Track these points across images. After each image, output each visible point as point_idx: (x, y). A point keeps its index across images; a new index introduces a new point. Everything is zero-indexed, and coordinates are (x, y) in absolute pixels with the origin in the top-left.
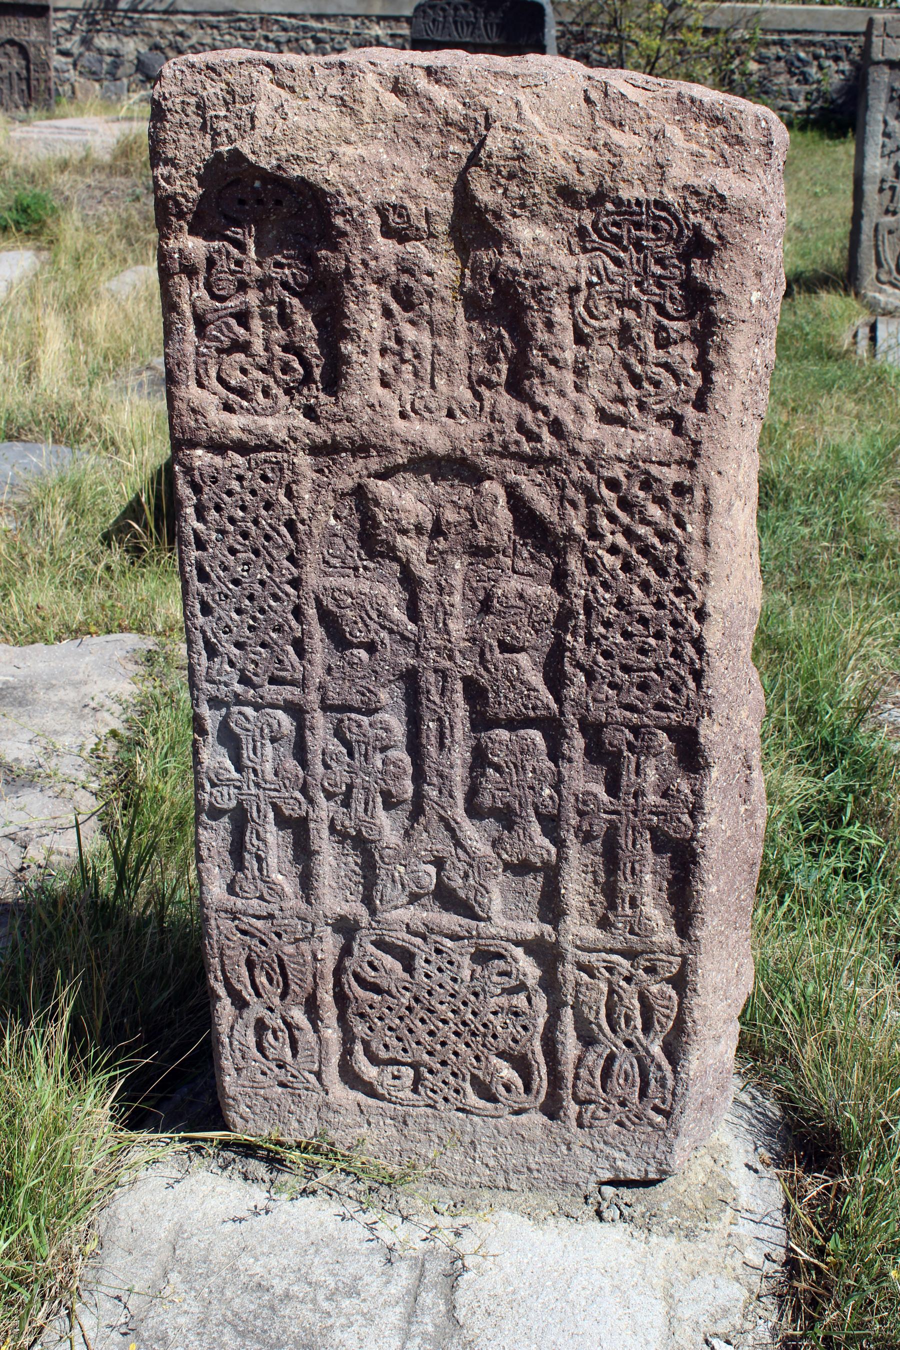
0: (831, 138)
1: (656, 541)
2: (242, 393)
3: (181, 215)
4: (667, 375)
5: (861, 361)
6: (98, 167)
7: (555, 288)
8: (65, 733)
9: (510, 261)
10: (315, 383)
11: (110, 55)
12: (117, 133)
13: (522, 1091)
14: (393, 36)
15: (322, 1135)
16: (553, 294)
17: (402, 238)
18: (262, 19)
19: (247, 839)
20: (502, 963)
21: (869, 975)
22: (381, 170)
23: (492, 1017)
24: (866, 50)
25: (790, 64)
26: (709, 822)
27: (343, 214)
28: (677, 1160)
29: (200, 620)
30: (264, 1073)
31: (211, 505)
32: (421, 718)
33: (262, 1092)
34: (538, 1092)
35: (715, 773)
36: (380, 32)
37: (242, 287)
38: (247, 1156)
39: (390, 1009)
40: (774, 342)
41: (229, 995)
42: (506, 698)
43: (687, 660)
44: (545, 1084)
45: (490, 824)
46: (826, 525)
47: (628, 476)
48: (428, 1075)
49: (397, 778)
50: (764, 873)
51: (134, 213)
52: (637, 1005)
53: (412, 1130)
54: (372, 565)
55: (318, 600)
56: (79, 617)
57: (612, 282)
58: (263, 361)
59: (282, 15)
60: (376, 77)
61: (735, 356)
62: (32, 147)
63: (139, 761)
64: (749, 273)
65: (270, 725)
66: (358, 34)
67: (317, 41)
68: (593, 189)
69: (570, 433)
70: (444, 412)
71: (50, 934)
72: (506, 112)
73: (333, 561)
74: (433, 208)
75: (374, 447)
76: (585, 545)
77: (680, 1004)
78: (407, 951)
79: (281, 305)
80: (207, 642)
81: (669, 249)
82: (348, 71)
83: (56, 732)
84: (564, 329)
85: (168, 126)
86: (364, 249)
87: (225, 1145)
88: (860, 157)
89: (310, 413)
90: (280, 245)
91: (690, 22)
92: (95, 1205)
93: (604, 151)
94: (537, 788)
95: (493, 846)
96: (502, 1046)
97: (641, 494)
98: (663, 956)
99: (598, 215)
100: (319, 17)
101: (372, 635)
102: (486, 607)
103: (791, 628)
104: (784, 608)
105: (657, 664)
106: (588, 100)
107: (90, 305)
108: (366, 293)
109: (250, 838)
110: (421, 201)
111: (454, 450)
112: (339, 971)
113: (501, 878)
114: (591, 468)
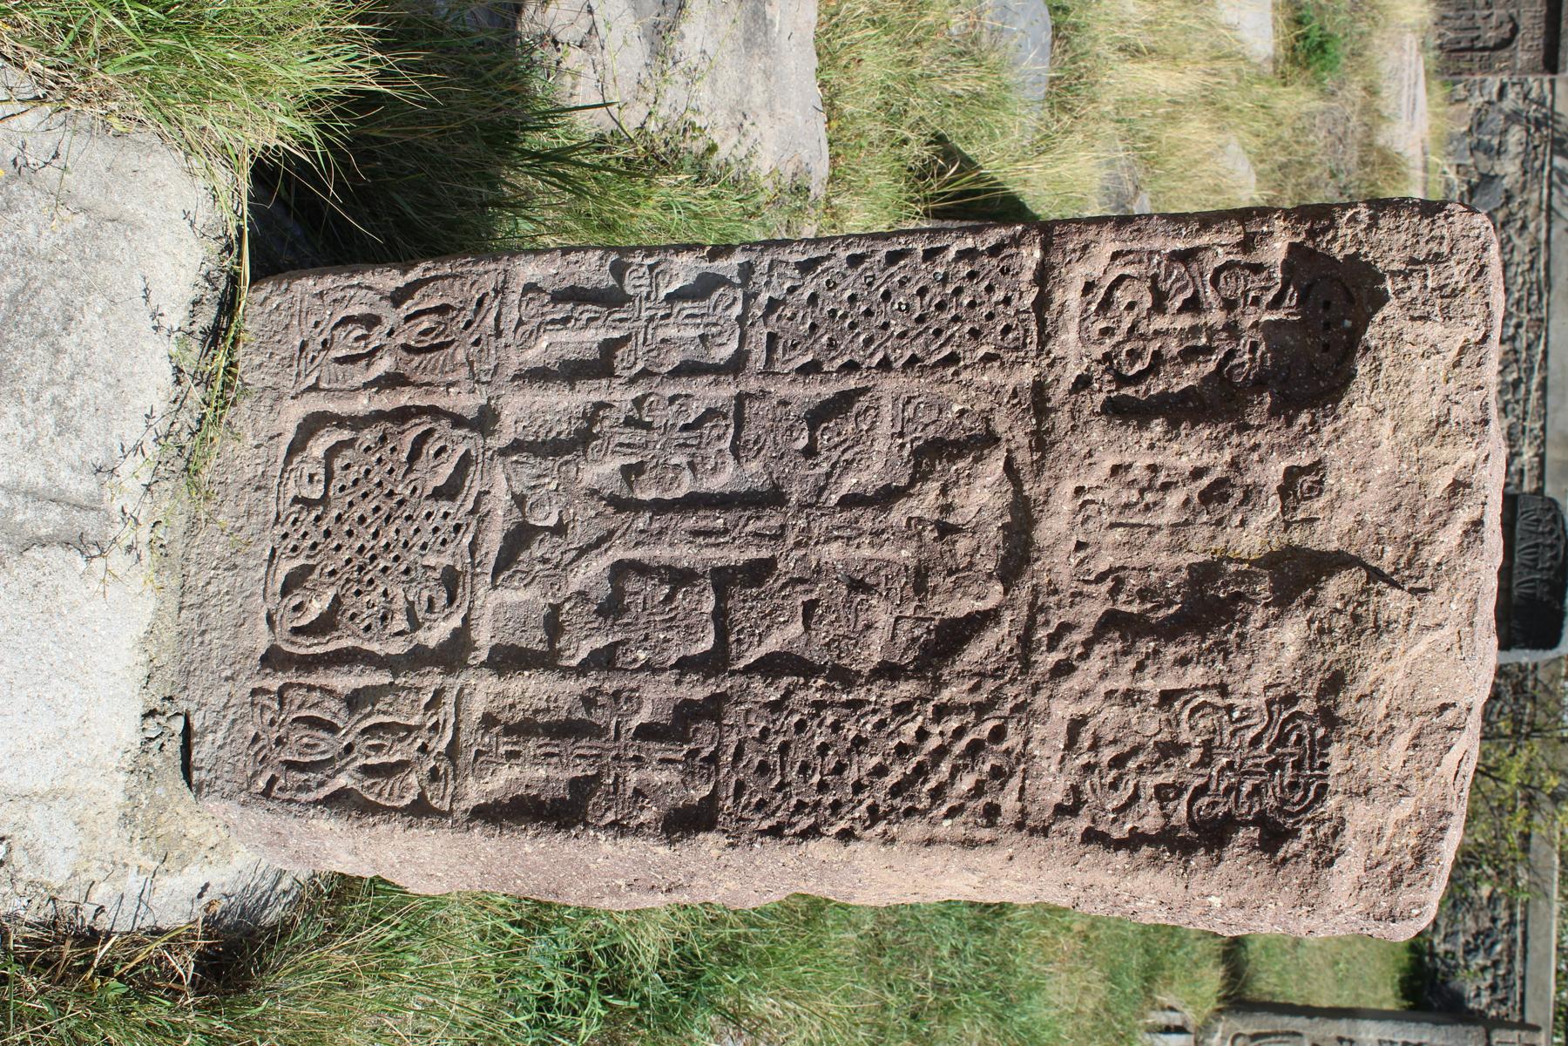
0: (1402, 981)
1: (932, 784)
2: (1106, 304)
3: (1312, 234)
4: (1125, 798)
5: (1142, 1016)
6: (1370, 130)
7: (1225, 668)
8: (713, 92)
9: (1258, 616)
10: (1117, 389)
11: (1500, 143)
12: (1408, 154)
13: (295, 624)
14: (1521, 472)
15: (245, 392)
16: (1219, 666)
17: (1285, 491)
18: (1541, 320)
19: (589, 307)
20: (444, 601)
21: (429, 1026)
22: (1363, 467)
23: (381, 590)
24: (1501, 1023)
25: (1488, 933)
26: (606, 844)
27: (1313, 423)
28: (213, 804)
29: (843, 254)
30: (317, 324)
31: (976, 268)
32: (727, 510)
33: (295, 322)
34: (293, 643)
35: (663, 851)
36: (1525, 457)
37: (1229, 305)
38: (221, 304)
39: (391, 471)
40: (1163, 921)
41: (408, 285)
42: (751, 608)
43: (794, 820)
44: (303, 651)
45: (605, 589)
46: (952, 976)
47: (1008, 752)
48: (313, 515)
49: (659, 481)
50: (549, 906)
51: (1317, 172)
52: (394, 759)
53: (250, 496)
54: (906, 453)
55: (865, 390)
56: (848, 109)
57: (1233, 734)
58: (1142, 329)
59: (1546, 344)
60: (1471, 462)
61: (1146, 876)
62: (1394, 54)
63: (680, 178)
64: (1242, 894)
65: (720, 334)
66: (1523, 432)
67: (1516, 384)
68: (1341, 713)
69: (1058, 685)
70: (1082, 539)
71: (481, 75)
72: (1430, 613)
73: (910, 409)
74: (1320, 527)
75: (1043, 457)
76: (928, 701)
77: (395, 809)
78: (458, 493)
79: (1208, 350)
80: (815, 262)
81: (1270, 802)
82: (1478, 430)
83: (714, 81)
84: (1179, 679)
85: (1416, 220)
86: (1272, 447)
87: (234, 279)
88: (1380, 1016)
89: (1083, 383)
90: (1276, 350)
91: (1537, 819)
92: (165, 128)
93: (1385, 725)
94: (646, 644)
95: (579, 593)
96: (346, 601)
97: (987, 767)
98: (450, 790)
99: (1311, 719)
100: (1543, 386)
101: (824, 453)
102: (857, 585)
103: (833, 936)
104: (856, 927)
105: (789, 784)
106: (1444, 708)
107: (1210, 121)
108: (1220, 448)
109: (590, 310)
110: (1327, 513)
111: (1039, 550)
112: (435, 412)
113: (542, 601)
114: (1018, 708)
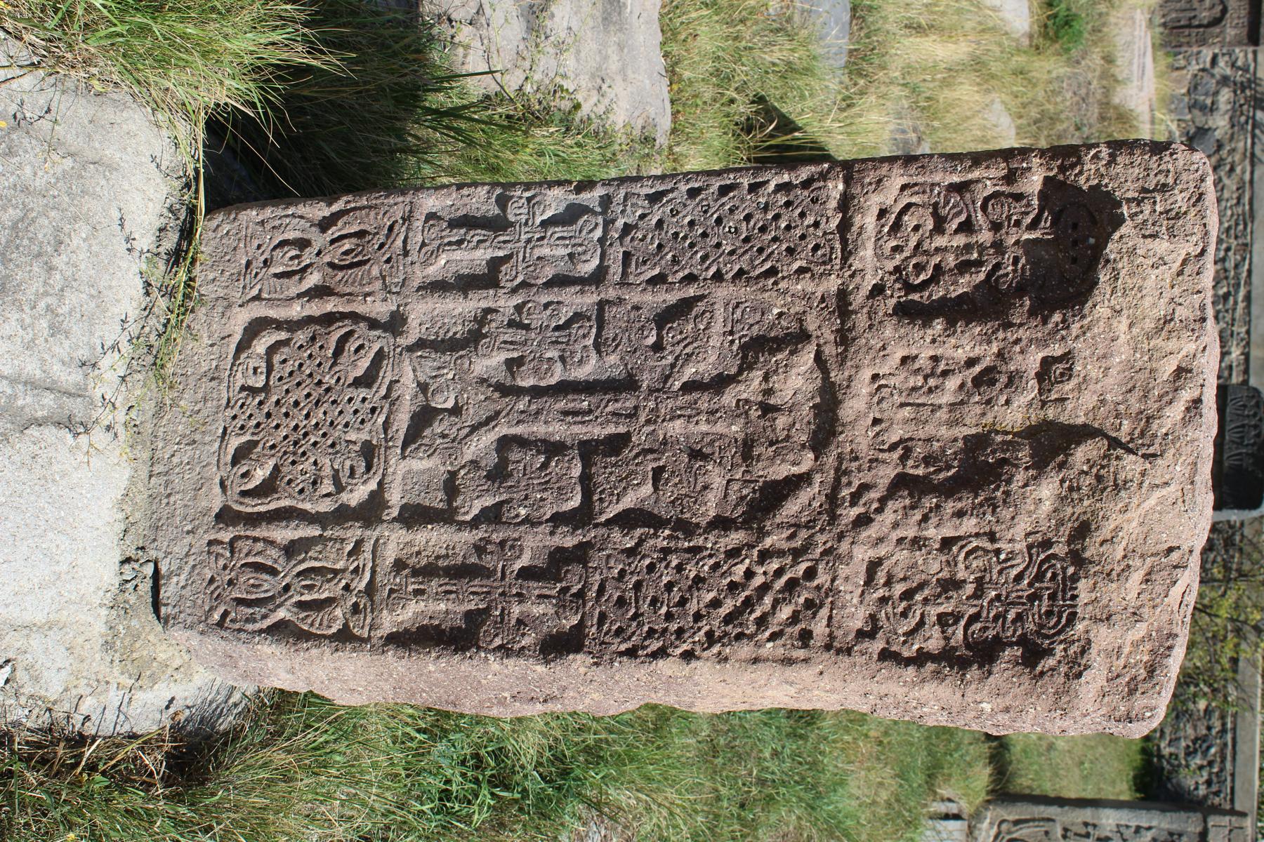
67: (1226, 297)
100: (1248, 298)
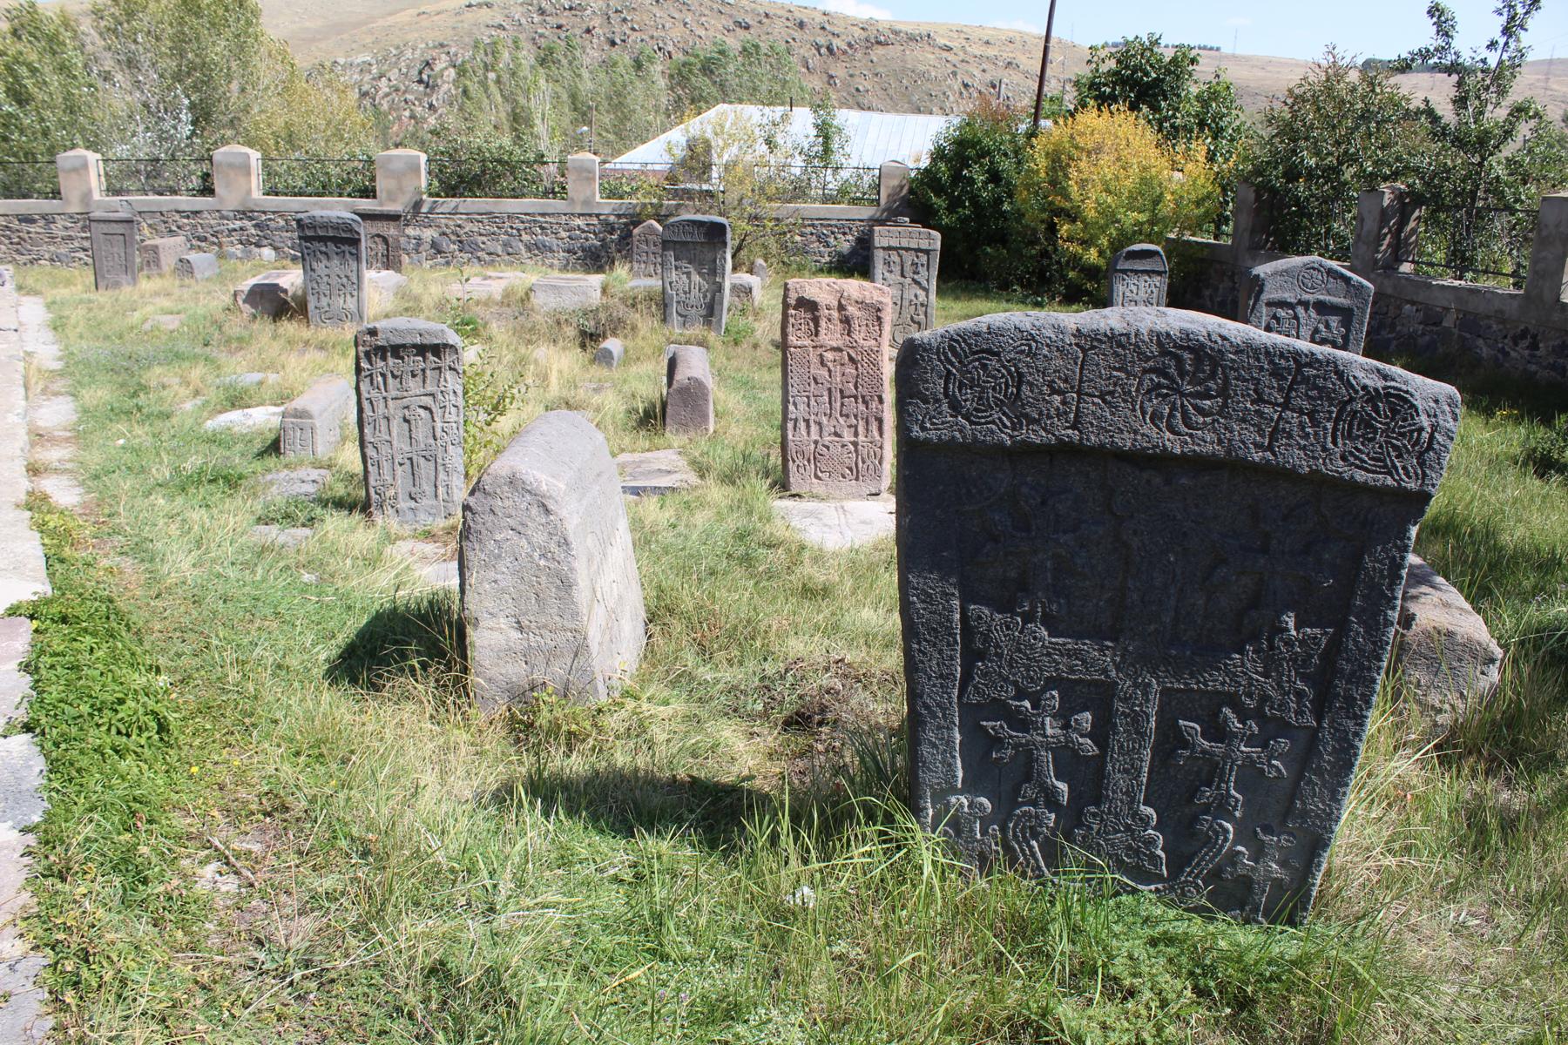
67: (542, 228)
100: (543, 215)
